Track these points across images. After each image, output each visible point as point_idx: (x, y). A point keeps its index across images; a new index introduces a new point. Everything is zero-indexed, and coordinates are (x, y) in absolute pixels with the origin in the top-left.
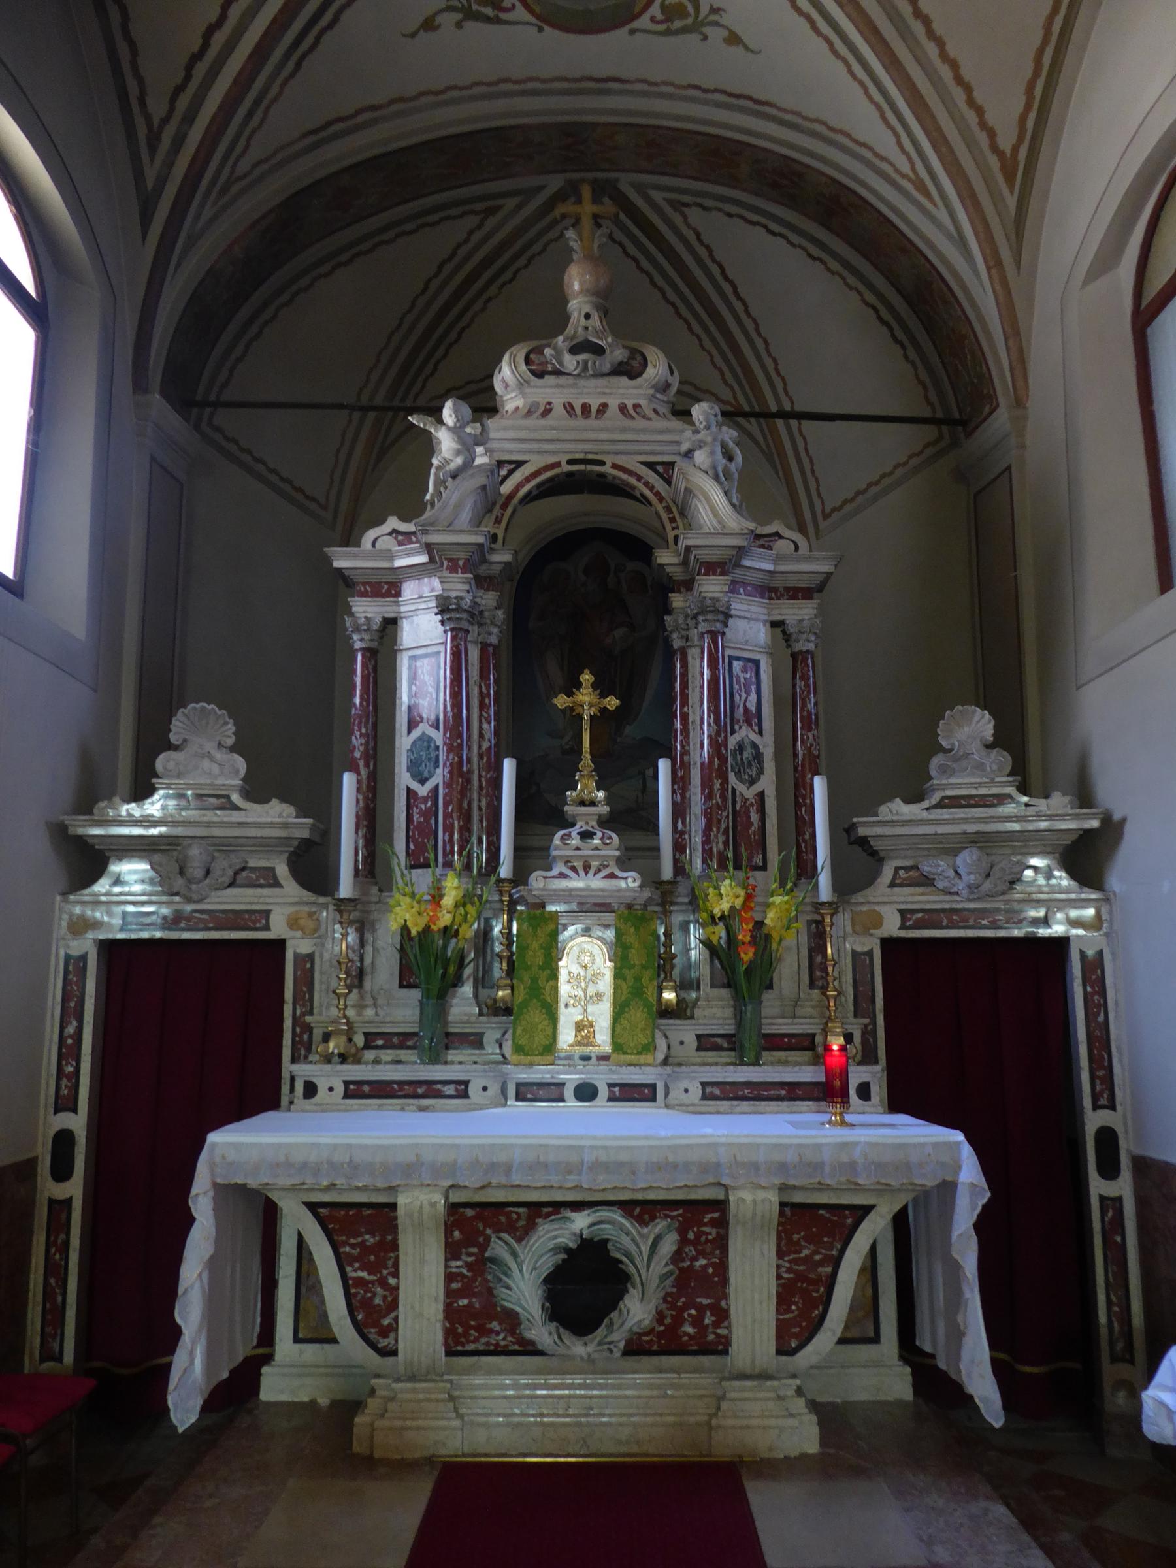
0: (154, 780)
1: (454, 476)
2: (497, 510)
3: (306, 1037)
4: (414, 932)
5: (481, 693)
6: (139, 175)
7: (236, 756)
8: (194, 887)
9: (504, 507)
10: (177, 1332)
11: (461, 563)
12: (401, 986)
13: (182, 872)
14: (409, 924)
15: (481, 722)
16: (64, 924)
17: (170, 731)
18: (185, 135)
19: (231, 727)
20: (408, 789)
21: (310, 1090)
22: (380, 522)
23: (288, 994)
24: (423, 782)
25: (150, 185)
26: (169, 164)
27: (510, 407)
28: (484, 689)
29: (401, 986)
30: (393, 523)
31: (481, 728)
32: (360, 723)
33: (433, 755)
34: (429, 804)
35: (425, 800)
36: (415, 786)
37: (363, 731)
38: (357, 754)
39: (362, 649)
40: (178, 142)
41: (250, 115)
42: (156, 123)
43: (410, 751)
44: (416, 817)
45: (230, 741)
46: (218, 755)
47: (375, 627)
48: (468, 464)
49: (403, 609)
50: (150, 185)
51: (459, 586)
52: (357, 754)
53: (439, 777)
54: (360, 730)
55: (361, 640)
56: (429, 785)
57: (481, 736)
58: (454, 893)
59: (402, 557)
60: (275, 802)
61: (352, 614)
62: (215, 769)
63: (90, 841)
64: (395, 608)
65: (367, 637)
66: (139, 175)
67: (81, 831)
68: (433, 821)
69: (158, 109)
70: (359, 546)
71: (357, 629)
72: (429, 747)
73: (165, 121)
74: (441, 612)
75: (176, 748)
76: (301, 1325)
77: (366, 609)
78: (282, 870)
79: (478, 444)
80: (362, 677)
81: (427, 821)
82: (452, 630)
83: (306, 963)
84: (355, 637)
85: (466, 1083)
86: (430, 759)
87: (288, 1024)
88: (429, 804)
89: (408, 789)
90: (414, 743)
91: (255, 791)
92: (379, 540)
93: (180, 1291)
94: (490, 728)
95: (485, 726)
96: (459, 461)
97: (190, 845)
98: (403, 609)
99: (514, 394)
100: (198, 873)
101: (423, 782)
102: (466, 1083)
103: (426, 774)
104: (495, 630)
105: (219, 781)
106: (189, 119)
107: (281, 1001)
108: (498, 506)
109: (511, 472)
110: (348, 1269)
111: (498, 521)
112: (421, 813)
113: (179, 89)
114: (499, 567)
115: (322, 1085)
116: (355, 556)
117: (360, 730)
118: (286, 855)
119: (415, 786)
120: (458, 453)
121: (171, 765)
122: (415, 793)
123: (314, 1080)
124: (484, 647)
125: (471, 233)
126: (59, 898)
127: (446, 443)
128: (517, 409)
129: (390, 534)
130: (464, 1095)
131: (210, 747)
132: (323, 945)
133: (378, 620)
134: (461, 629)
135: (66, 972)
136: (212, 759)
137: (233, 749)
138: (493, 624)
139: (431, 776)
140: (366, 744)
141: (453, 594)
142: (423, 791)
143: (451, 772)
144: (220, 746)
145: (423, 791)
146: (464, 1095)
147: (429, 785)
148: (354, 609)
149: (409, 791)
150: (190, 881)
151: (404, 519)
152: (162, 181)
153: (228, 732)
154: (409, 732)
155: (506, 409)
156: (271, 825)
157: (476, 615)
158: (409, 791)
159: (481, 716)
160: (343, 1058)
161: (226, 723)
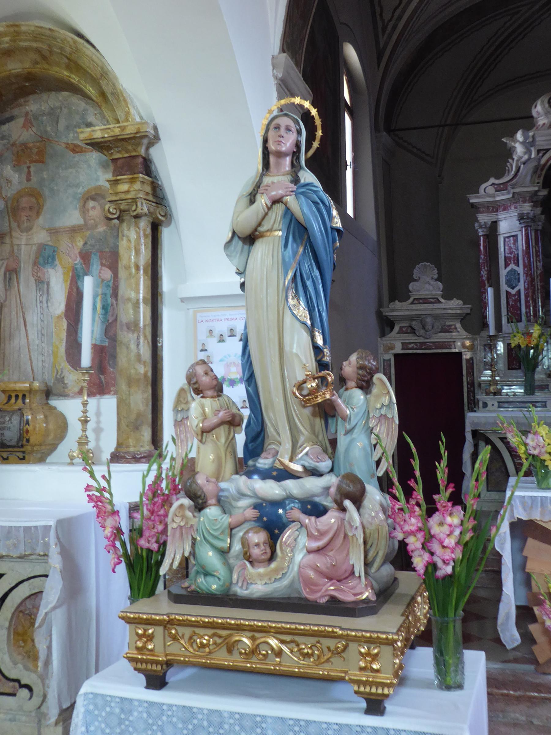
0: (410, 294)
1: (524, 164)
2: (539, 172)
3: (472, 389)
4: (522, 346)
5: (536, 250)
6: (377, 43)
7: (439, 282)
8: (427, 333)
9: (542, 170)
10: (464, 474)
11: (527, 198)
12: (509, 369)
13: (424, 328)
14: (520, 344)
15: (536, 263)
16: (382, 348)
17: (413, 274)
18: (397, 25)
19: (436, 271)
20: (507, 292)
21: (485, 405)
22: (487, 180)
23: (464, 372)
24: (513, 288)
25: (381, 46)
26: (390, 37)
27: (541, 123)
28: (537, 249)
29: (509, 369)
30: (492, 180)
31: (537, 265)
32: (484, 266)
33: (517, 277)
34: (516, 297)
35: (514, 295)
36: (509, 290)
37: (486, 269)
38: (484, 278)
39: (482, 235)
40: (395, 27)
41: (422, 10)
42: (386, 21)
43: (507, 276)
44: (511, 303)
45: (436, 277)
46: (433, 282)
47: (488, 226)
48: (530, 158)
49: (500, 217)
50: (381, 46)
51: (527, 208)
52: (484, 278)
53: (521, 286)
54: (484, 268)
55: (483, 231)
56: (516, 289)
57: (537, 268)
58: (538, 332)
59: (499, 196)
60: (455, 299)
61: (478, 221)
62: (431, 288)
63: (389, 317)
64: (496, 217)
65: (485, 230)
66: (377, 43)
67: (387, 314)
68: (518, 304)
69: (387, 17)
70: (478, 193)
71: (481, 227)
72: (515, 274)
73: (390, 20)
74: (519, 220)
75: (415, 280)
76: (489, 486)
77: (484, 218)
78: (458, 325)
79: (532, 146)
80: (484, 246)
81: (516, 304)
82: (525, 227)
83: (470, 362)
84: (480, 230)
85: (545, 402)
86: (515, 279)
87: (465, 384)
88: (516, 297)
89: (507, 292)
90: (508, 273)
91: (448, 296)
92: (487, 189)
93: (464, 462)
94: (540, 265)
95: (538, 264)
96: (526, 157)
97: (426, 317)
98: (500, 217)
99: (542, 118)
100: (430, 328)
101: (513, 288)
102: (545, 402)
103: (514, 285)
104: (540, 223)
105: (434, 293)
106: (400, 18)
107: (462, 375)
108: (539, 170)
109: (544, 154)
110: (515, 460)
111: (539, 177)
112: (513, 301)
113: (396, 8)
114: (541, 197)
115: (489, 404)
116: (479, 197)
117: (484, 268)
118: (460, 320)
119: (509, 290)
120: (525, 153)
121: (415, 287)
122: (510, 293)
123: (486, 402)
124: (536, 231)
125: (506, 23)
126: (379, 339)
127: (519, 149)
128: (544, 124)
129: (491, 185)
130: (545, 406)
131: (428, 279)
132: (476, 354)
133: (489, 223)
134: (529, 226)
135: (384, 366)
136: (430, 284)
137: (437, 280)
138: (539, 221)
139: (516, 286)
140: (488, 274)
141: (525, 212)
142: (513, 292)
143: (528, 285)
144: (432, 278)
145: (513, 292)
146: (545, 406)
147: (516, 289)
148: (479, 219)
149: (508, 293)
150: (426, 331)
151: (497, 178)
152: (386, 44)
153: (435, 273)
154: (506, 268)
155: (539, 123)
156: (456, 308)
157: (534, 219)
158: (508, 293)
159: (536, 260)
160: (495, 394)
161: (434, 270)
